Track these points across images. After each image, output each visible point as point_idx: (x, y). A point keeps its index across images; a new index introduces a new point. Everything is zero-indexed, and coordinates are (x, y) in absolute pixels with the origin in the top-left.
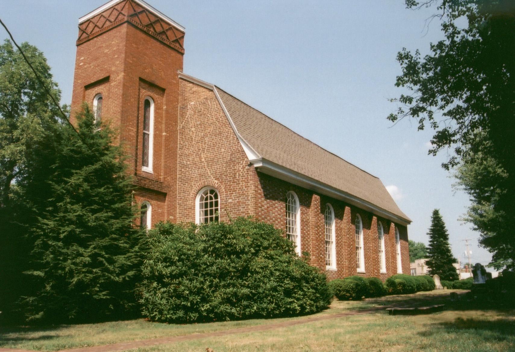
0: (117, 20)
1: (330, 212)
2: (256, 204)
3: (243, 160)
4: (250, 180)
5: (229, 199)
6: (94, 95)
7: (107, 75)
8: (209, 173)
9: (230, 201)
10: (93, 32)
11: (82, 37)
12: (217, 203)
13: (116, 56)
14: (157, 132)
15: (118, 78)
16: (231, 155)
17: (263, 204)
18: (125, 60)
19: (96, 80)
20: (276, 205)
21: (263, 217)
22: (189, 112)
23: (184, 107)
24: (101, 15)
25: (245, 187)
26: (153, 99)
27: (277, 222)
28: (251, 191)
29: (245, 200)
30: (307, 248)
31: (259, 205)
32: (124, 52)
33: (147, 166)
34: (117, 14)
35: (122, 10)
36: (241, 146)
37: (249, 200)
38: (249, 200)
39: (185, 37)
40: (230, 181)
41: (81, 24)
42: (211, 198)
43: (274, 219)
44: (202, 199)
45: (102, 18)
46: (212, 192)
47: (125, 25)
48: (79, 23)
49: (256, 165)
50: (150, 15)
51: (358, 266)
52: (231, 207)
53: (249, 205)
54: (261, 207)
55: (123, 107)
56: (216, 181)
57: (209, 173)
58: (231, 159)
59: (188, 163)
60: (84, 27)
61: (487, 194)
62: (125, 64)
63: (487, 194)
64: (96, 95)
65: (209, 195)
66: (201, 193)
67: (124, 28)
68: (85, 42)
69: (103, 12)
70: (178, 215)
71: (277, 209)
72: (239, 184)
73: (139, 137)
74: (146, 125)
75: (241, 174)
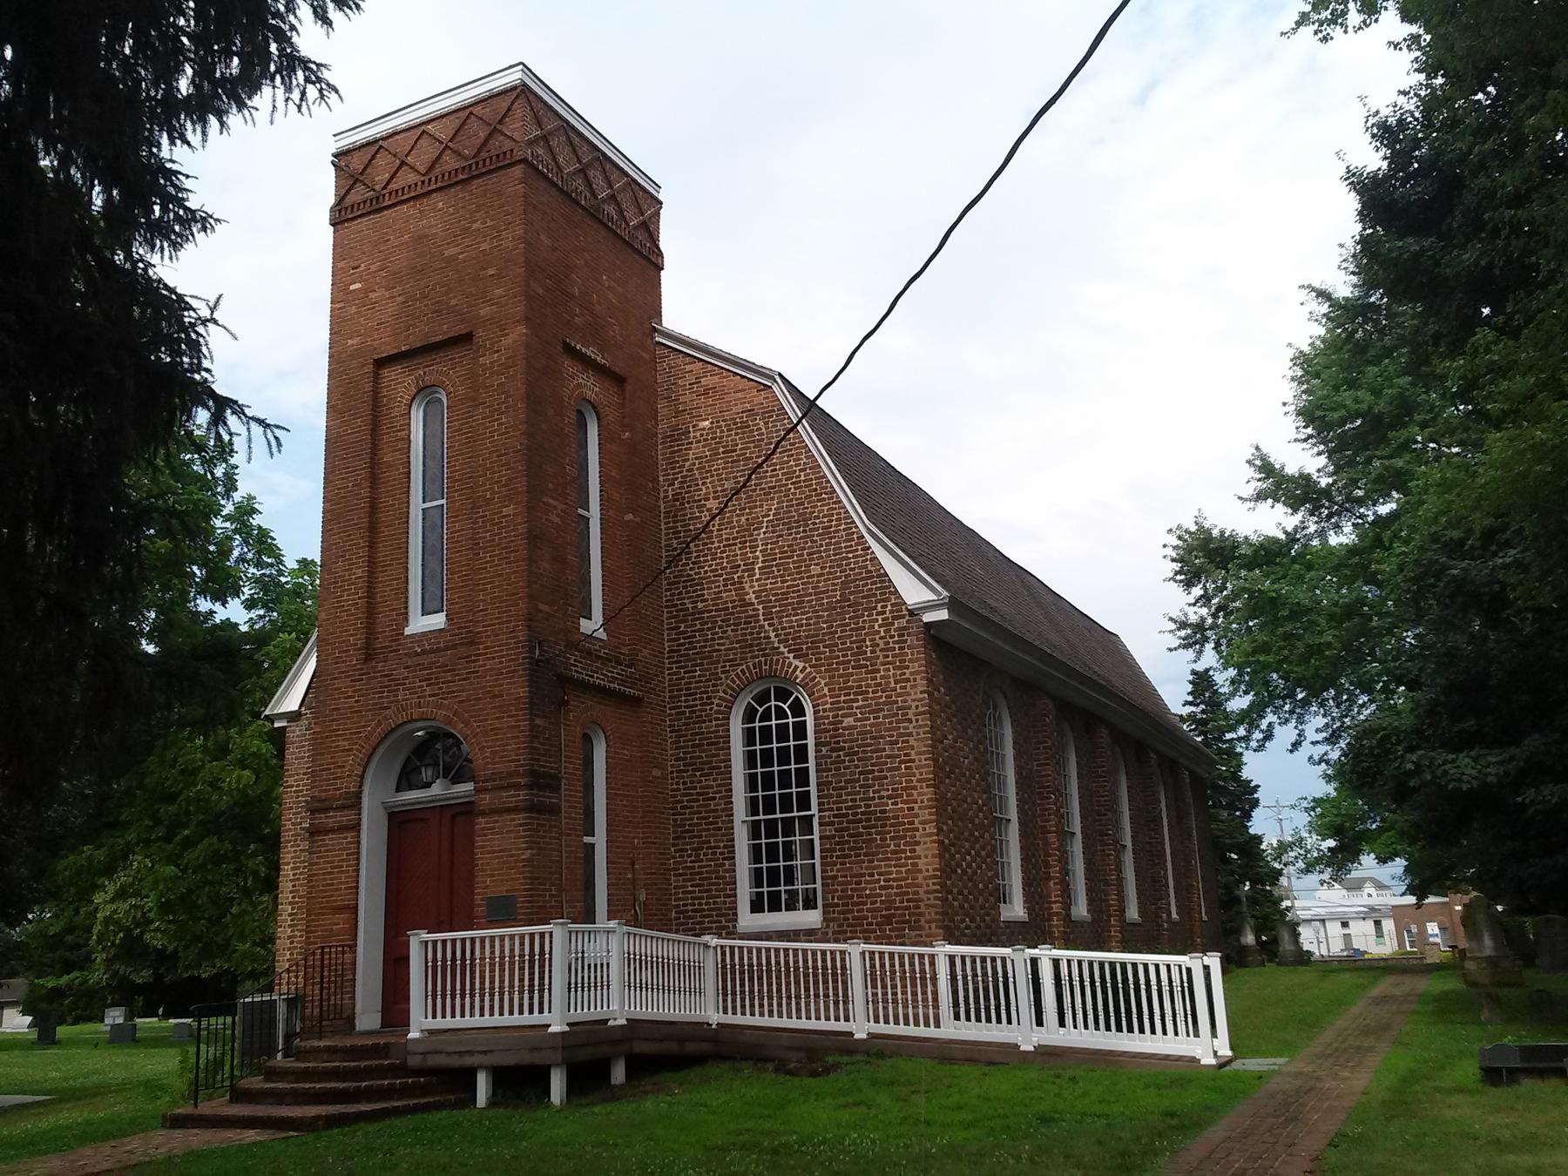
0: (484, 155)
1: (1000, 718)
3: (888, 600)
4: (911, 661)
5: (844, 716)
9: (849, 721)
10: (393, 186)
11: (349, 200)
13: (491, 272)
14: (611, 513)
23: (678, 436)
26: (597, 414)
28: (916, 694)
34: (482, 135)
37: (910, 721)
38: (910, 721)
40: (843, 663)
44: (750, 715)
45: (424, 142)
47: (518, 171)
49: (928, 617)
50: (577, 140)
52: (851, 741)
53: (910, 734)
58: (844, 598)
59: (700, 605)
60: (357, 163)
61: (157, 208)
63: (157, 208)
72: (878, 671)
75: (881, 643)
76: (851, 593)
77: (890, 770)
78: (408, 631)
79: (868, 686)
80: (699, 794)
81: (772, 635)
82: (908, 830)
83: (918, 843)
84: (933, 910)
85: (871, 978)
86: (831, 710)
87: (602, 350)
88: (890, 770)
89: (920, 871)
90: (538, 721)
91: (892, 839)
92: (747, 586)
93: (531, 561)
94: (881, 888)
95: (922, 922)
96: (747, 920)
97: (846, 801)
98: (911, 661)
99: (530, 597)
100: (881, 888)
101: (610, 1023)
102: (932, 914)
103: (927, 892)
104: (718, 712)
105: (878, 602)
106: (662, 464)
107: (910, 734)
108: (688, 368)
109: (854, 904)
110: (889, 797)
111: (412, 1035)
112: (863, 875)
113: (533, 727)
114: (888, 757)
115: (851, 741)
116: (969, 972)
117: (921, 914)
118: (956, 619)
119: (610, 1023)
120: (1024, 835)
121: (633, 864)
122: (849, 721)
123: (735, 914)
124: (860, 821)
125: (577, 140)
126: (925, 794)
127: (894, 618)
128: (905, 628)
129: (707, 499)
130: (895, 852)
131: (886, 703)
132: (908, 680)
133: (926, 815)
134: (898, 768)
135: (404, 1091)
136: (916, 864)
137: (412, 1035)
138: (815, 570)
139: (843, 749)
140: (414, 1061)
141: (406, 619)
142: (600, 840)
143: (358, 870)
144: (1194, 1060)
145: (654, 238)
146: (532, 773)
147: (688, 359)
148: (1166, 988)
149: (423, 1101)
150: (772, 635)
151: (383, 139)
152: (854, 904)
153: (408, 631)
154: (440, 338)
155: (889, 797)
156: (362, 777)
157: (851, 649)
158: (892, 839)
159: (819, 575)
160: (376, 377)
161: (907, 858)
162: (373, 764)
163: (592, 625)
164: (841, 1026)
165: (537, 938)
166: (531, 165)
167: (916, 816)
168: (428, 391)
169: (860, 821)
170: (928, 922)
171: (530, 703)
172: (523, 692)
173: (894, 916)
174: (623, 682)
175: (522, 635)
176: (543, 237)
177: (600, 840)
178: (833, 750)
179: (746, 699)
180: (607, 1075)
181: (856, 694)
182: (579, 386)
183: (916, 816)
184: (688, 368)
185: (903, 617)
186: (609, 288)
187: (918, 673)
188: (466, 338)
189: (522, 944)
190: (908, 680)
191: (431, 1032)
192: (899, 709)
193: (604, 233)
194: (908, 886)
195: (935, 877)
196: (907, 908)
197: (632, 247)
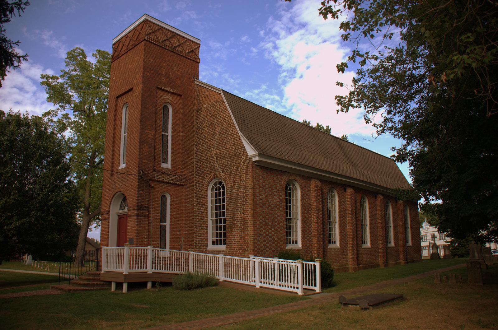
0: (138, 40)
2: (254, 194)
4: (249, 173)
5: (233, 189)
6: (123, 104)
7: (131, 87)
8: (218, 167)
9: (234, 191)
10: (122, 51)
12: (224, 192)
13: (137, 71)
14: (175, 133)
15: (138, 89)
16: (235, 150)
17: (261, 193)
18: (143, 73)
19: (123, 92)
20: (275, 193)
21: (261, 205)
22: (203, 113)
23: (199, 110)
24: (126, 36)
25: (246, 179)
27: (275, 208)
29: (246, 191)
30: (308, 229)
31: (258, 194)
32: (142, 67)
33: (167, 163)
35: (141, 30)
36: (242, 143)
37: (248, 191)
38: (248, 191)
39: (200, 48)
40: (233, 174)
41: (114, 45)
42: (220, 189)
43: (273, 206)
45: (128, 38)
46: (220, 183)
48: (113, 44)
49: (254, 159)
50: (166, 32)
51: (364, 242)
52: (234, 196)
53: (248, 195)
54: (259, 197)
55: (141, 114)
56: (223, 174)
57: (218, 167)
59: (202, 158)
62: (143, 77)
64: (124, 104)
65: (218, 186)
66: (212, 184)
67: (142, 46)
68: (116, 60)
69: (128, 33)
70: (195, 203)
71: (276, 197)
72: (241, 176)
73: (111, 153)
74: (166, 129)
75: (242, 167)
76: (236, 153)
77: (243, 205)
78: (119, 168)
79: (239, 180)
80: (200, 211)
81: (217, 166)
82: (246, 223)
83: (248, 227)
84: (251, 246)
85: (225, 265)
86: (230, 187)
87: (172, 88)
88: (243, 205)
89: (249, 235)
90: (141, 192)
91: (243, 225)
92: (213, 152)
93: (140, 148)
94: (240, 239)
95: (249, 250)
96: (211, 247)
97: (232, 214)
98: (249, 173)
99: (139, 158)
100: (240, 239)
101: (148, 273)
102: (251, 247)
103: (250, 241)
104: (205, 188)
105: (242, 155)
106: (195, 118)
107: (248, 195)
108: (202, 90)
109: (233, 244)
110: (242, 213)
111: (102, 272)
112: (235, 235)
113: (139, 194)
114: (243, 201)
115: (234, 196)
116: (239, 263)
117: (249, 247)
118: (262, 159)
119: (148, 273)
120: (340, 226)
121: (180, 230)
122: (234, 191)
123: (207, 245)
124: (235, 220)
125: (166, 32)
126: (251, 212)
127: (246, 160)
128: (248, 163)
129: (205, 127)
130: (243, 229)
131: (243, 185)
132: (248, 178)
133: (251, 218)
134: (245, 205)
135: (97, 285)
136: (248, 233)
137: (102, 272)
138: (228, 146)
139: (232, 199)
140: (102, 279)
141: (119, 165)
142: (168, 224)
143: (109, 230)
144: (297, 293)
145: (197, 55)
146: (138, 206)
147: (202, 88)
148: (289, 272)
149: (90, 288)
150: (217, 166)
151: (121, 39)
152: (233, 244)
153: (119, 168)
154: (127, 90)
155: (242, 213)
156: (110, 206)
157: (235, 169)
158: (243, 225)
159: (229, 148)
160: (116, 102)
161: (246, 231)
162: (112, 203)
163: (168, 165)
164: (145, 270)
165: (137, 250)
166: (147, 41)
167: (248, 219)
168: (126, 104)
169: (235, 220)
170: (250, 249)
171: (138, 187)
172: (137, 184)
173: (242, 247)
174: (176, 180)
175: (137, 169)
176: (151, 59)
177: (168, 224)
178: (230, 199)
179: (212, 184)
180: (146, 286)
181: (236, 183)
182: (165, 99)
183: (248, 219)
184: (202, 90)
185: (248, 160)
186: (177, 71)
187: (251, 176)
188: (131, 90)
189: (136, 251)
190: (248, 178)
191: (225, 281)
192: (246, 187)
193: (176, 55)
194: (246, 239)
195: (252, 236)
196: (245, 245)
197: (187, 58)
